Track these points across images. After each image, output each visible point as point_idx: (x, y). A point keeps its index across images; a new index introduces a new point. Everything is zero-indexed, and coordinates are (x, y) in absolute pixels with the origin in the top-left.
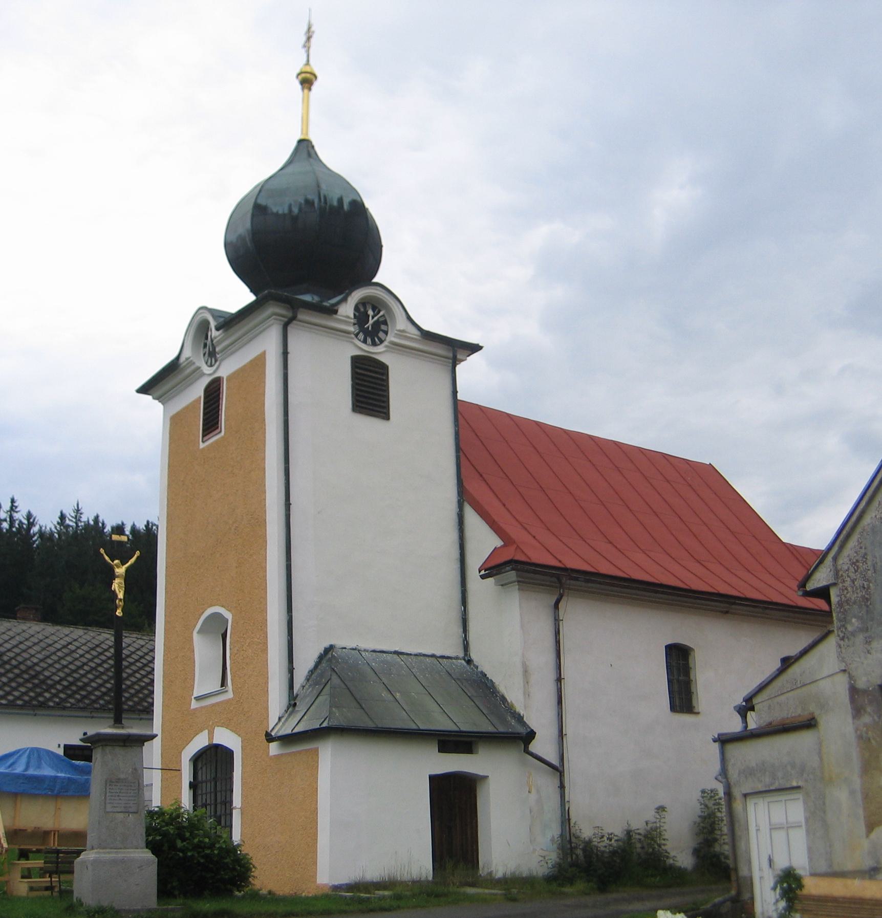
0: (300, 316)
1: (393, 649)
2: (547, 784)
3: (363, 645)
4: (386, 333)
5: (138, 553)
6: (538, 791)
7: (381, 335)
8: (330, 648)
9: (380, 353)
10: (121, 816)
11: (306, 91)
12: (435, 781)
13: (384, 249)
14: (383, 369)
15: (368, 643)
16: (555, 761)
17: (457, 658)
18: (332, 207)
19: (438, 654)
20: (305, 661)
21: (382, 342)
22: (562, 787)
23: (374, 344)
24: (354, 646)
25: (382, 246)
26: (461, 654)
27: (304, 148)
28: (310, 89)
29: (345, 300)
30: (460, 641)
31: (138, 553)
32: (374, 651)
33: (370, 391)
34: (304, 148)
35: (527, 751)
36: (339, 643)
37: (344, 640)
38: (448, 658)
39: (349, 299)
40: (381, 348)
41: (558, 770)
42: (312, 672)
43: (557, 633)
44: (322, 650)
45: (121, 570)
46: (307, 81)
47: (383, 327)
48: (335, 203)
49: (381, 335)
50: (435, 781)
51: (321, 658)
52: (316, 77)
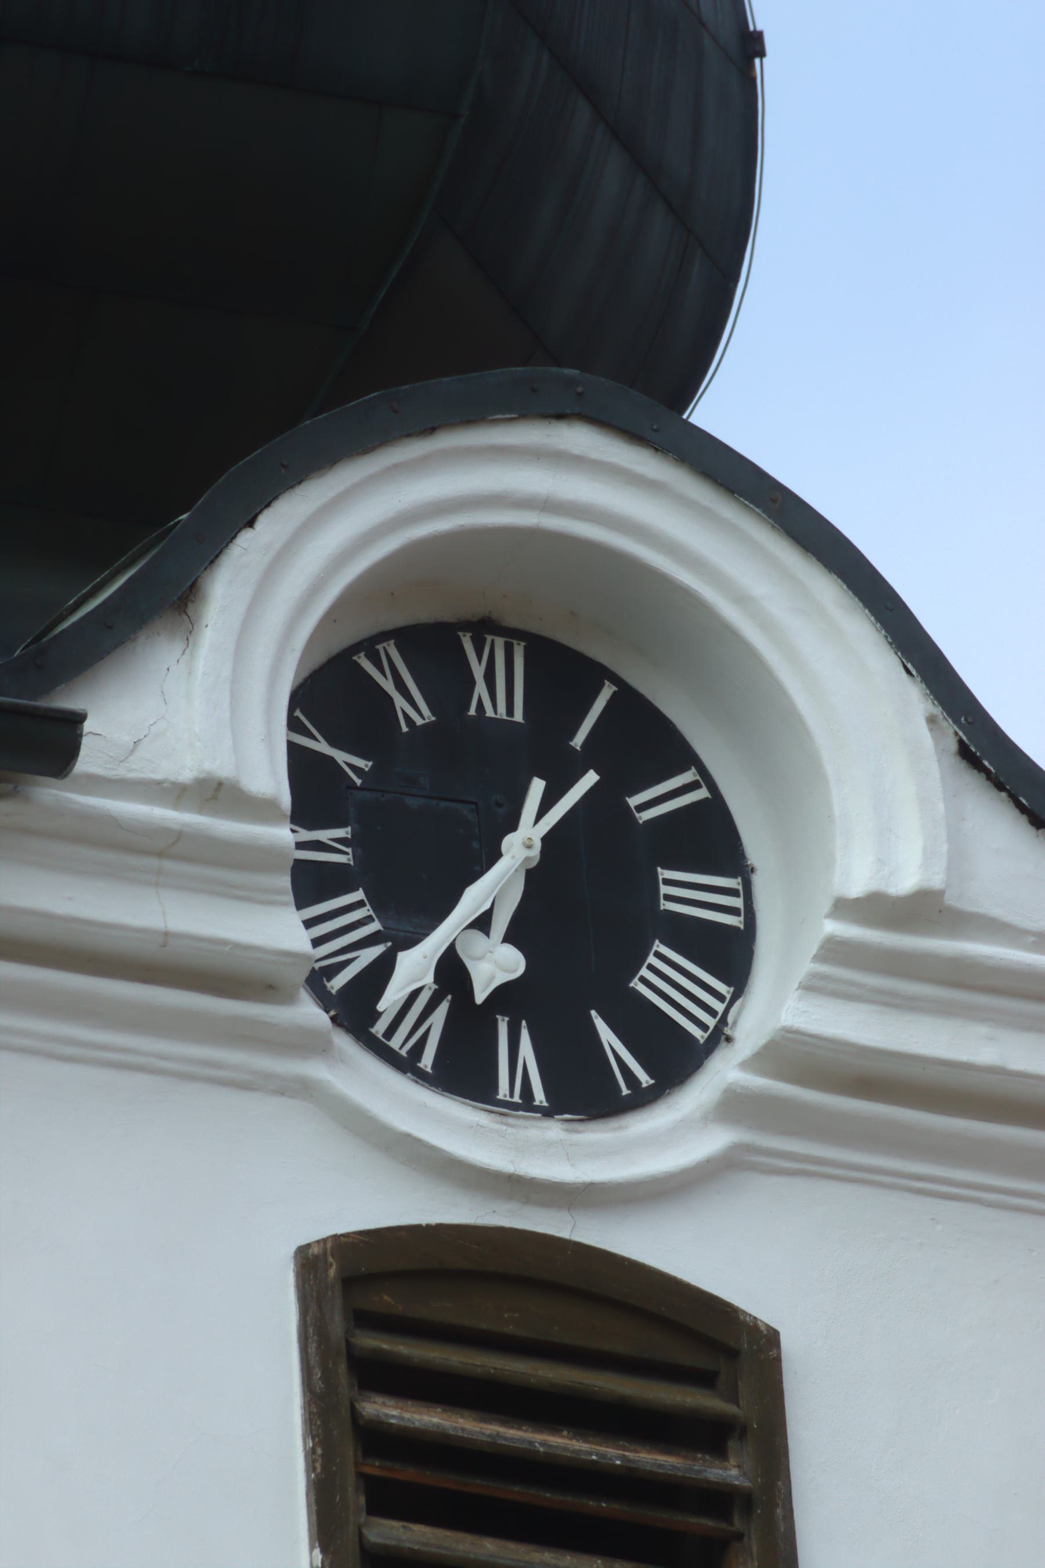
4: (729, 954)
7: (664, 977)
9: (659, 1187)
13: (777, 78)
14: (713, 1367)
21: (673, 1058)
23: (584, 1093)
40: (670, 1134)
47: (684, 891)
49: (664, 977)
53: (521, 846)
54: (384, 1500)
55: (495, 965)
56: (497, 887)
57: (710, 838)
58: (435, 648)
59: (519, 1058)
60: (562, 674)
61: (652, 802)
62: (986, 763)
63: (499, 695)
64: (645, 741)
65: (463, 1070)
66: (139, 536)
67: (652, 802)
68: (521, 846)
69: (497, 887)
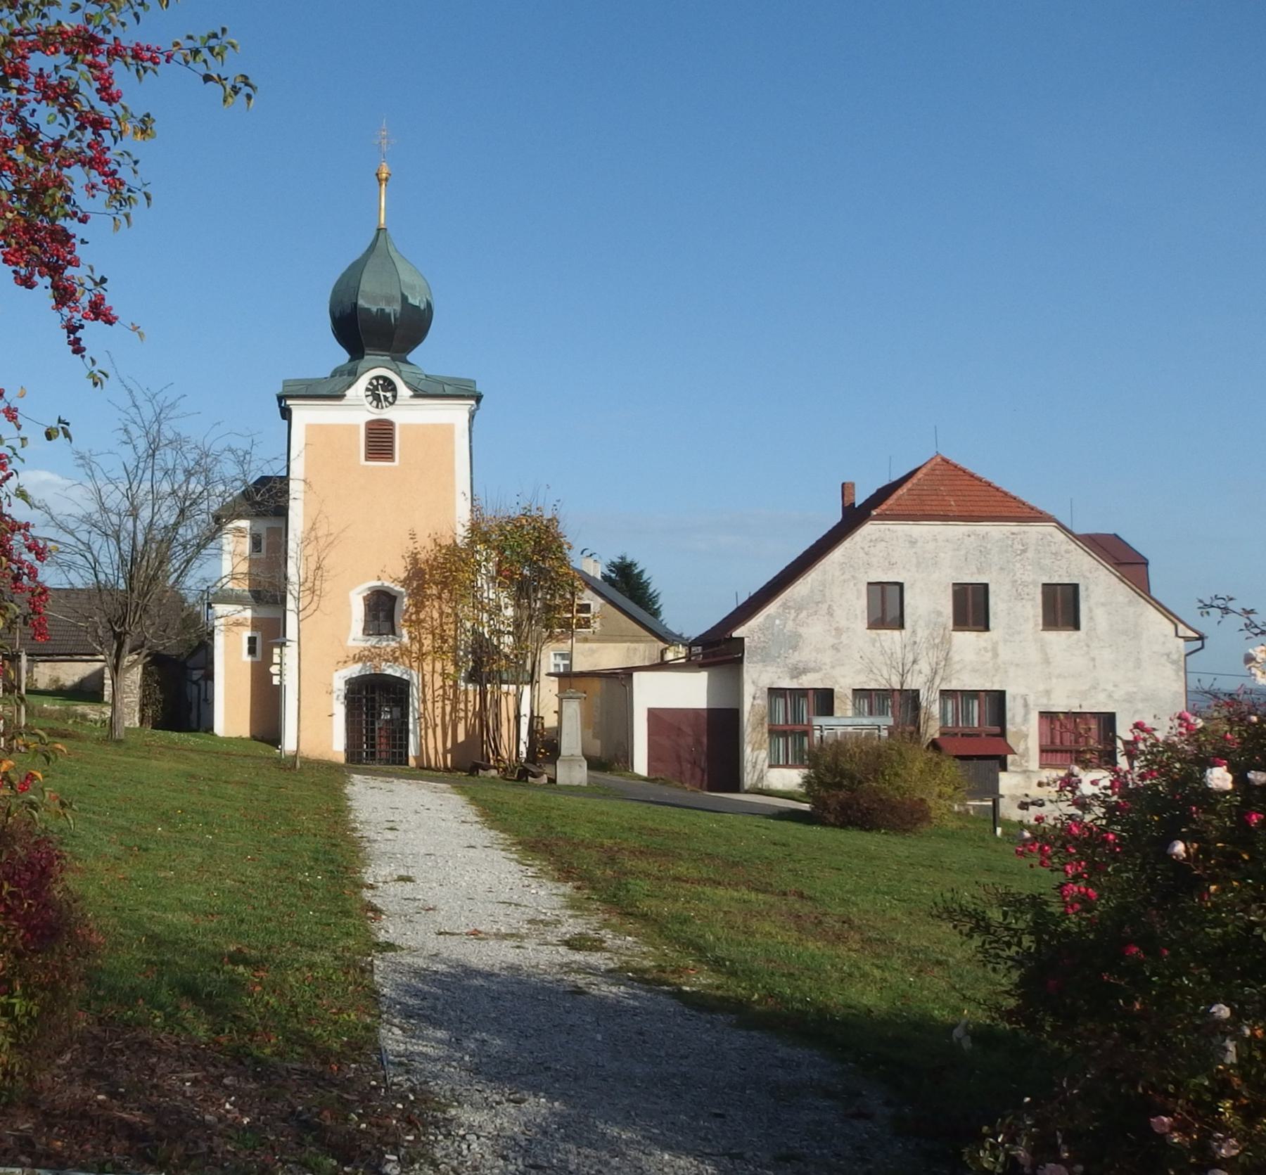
9: (388, 413)
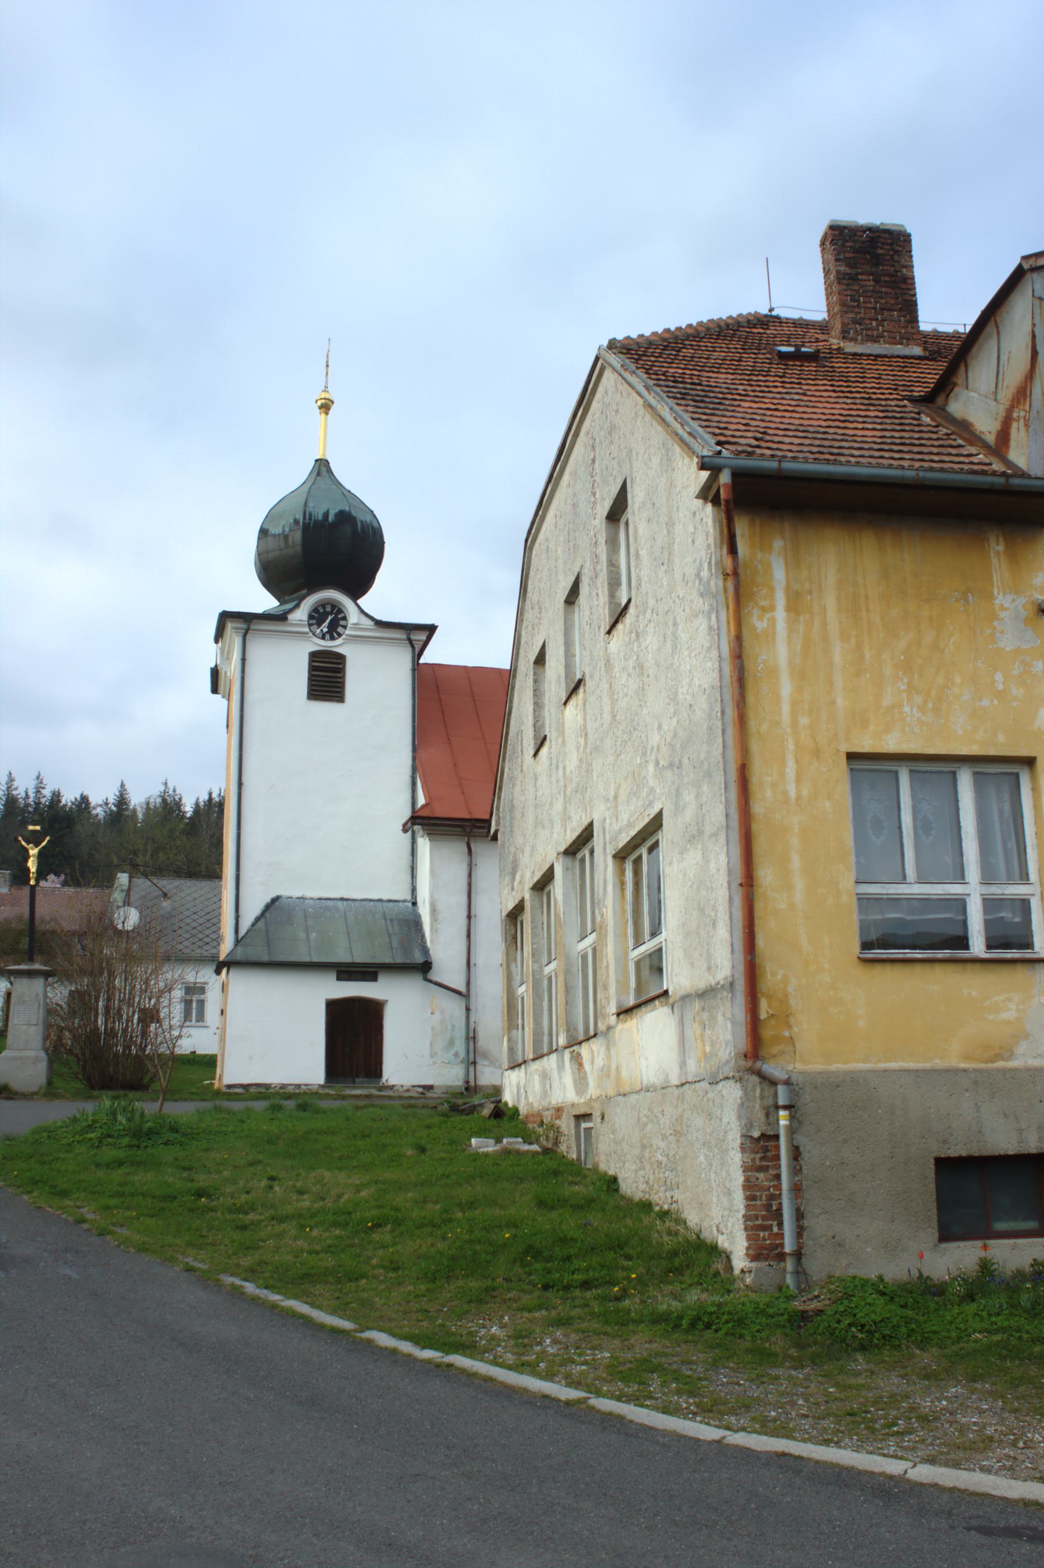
0: (252, 627)
1: (338, 896)
2: (454, 1007)
3: (309, 894)
4: (345, 627)
5: (48, 838)
6: (442, 1013)
7: (340, 630)
8: (275, 900)
9: (337, 646)
10: (25, 1027)
11: (323, 415)
12: (333, 1006)
13: (386, 546)
14: (341, 659)
15: (314, 892)
16: (462, 988)
17: (405, 901)
18: (316, 522)
19: (385, 897)
20: (252, 910)
21: (340, 635)
22: (468, 1009)
23: (332, 638)
24: (300, 895)
25: (384, 543)
26: (409, 897)
27: (322, 467)
28: (327, 414)
29: (297, 606)
30: (408, 886)
31: (48, 838)
32: (320, 899)
33: (327, 680)
34: (322, 467)
35: (426, 979)
36: (285, 893)
37: (291, 890)
38: (395, 901)
39: (302, 605)
40: (339, 641)
41: (465, 995)
42: (257, 919)
43: (470, 876)
44: (268, 900)
45: (33, 851)
46: (326, 407)
47: (342, 623)
48: (320, 518)
49: (340, 630)
50: (333, 1006)
51: (267, 907)
52: (333, 402)
53: (328, 621)
54: (314, 670)
55: (325, 630)
56: (326, 623)
57: (345, 618)
58: (324, 606)
59: (328, 636)
60: (333, 606)
61: (340, 616)
62: (383, 1339)
63: (328, 609)
64: (340, 611)
65: (323, 638)
66: (314, 587)
67: (340, 616)
68: (328, 621)
69: (326, 623)
